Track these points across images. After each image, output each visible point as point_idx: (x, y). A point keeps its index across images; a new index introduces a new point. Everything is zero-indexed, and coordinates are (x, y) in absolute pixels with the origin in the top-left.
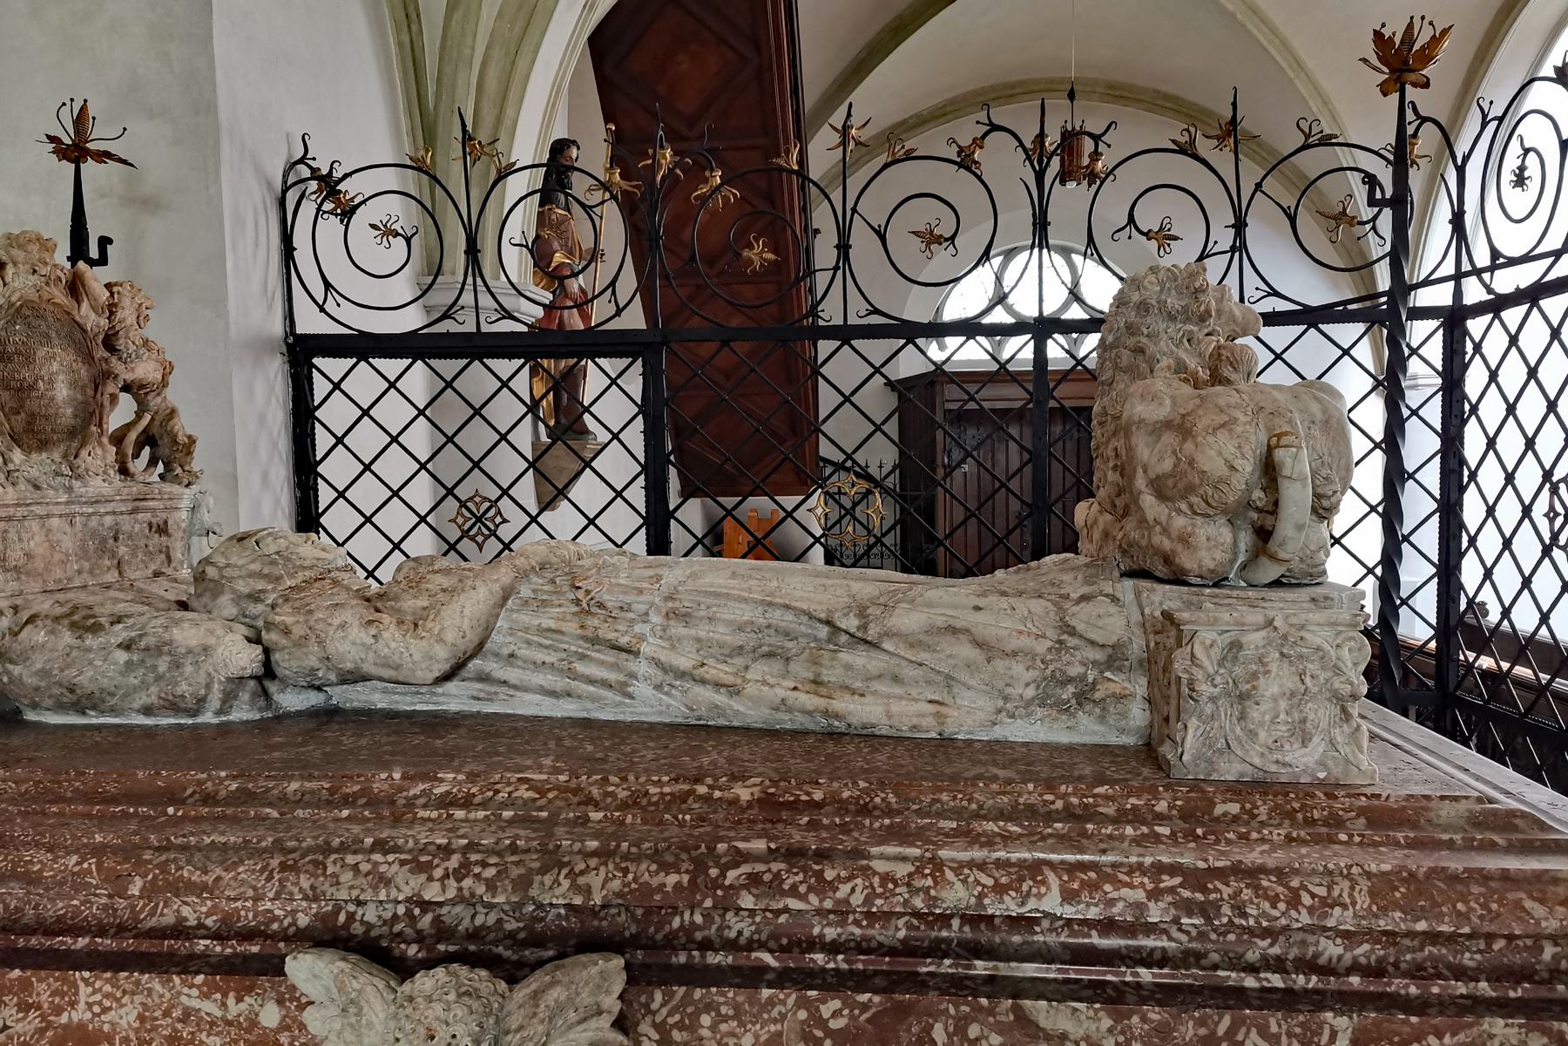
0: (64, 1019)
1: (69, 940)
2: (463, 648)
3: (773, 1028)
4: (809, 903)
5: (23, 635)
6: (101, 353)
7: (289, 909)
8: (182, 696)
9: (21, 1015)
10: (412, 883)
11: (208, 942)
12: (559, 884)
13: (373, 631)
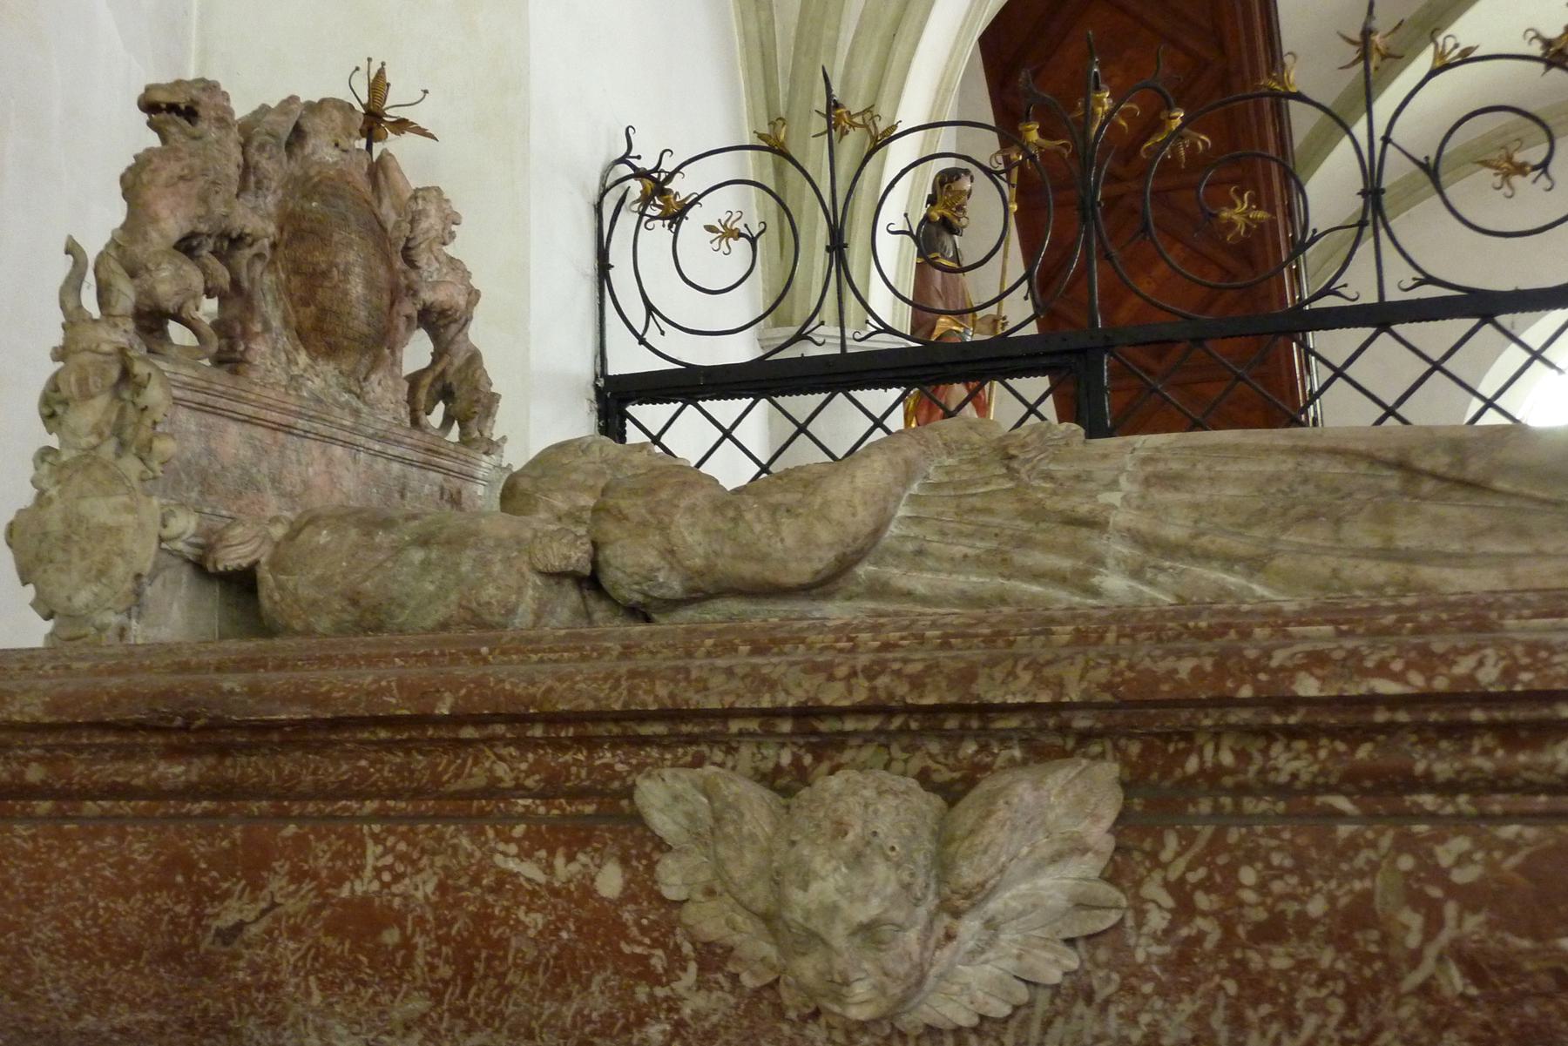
0: (345, 892)
1: (354, 805)
2: (852, 529)
3: (1358, 885)
4: (1407, 683)
5: (303, 537)
6: (399, 264)
7: (634, 761)
8: (489, 603)
9: (292, 888)
10: (806, 685)
11: (529, 802)
12: (1016, 677)
13: (731, 513)
